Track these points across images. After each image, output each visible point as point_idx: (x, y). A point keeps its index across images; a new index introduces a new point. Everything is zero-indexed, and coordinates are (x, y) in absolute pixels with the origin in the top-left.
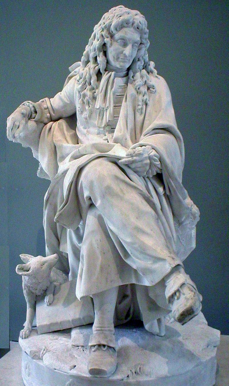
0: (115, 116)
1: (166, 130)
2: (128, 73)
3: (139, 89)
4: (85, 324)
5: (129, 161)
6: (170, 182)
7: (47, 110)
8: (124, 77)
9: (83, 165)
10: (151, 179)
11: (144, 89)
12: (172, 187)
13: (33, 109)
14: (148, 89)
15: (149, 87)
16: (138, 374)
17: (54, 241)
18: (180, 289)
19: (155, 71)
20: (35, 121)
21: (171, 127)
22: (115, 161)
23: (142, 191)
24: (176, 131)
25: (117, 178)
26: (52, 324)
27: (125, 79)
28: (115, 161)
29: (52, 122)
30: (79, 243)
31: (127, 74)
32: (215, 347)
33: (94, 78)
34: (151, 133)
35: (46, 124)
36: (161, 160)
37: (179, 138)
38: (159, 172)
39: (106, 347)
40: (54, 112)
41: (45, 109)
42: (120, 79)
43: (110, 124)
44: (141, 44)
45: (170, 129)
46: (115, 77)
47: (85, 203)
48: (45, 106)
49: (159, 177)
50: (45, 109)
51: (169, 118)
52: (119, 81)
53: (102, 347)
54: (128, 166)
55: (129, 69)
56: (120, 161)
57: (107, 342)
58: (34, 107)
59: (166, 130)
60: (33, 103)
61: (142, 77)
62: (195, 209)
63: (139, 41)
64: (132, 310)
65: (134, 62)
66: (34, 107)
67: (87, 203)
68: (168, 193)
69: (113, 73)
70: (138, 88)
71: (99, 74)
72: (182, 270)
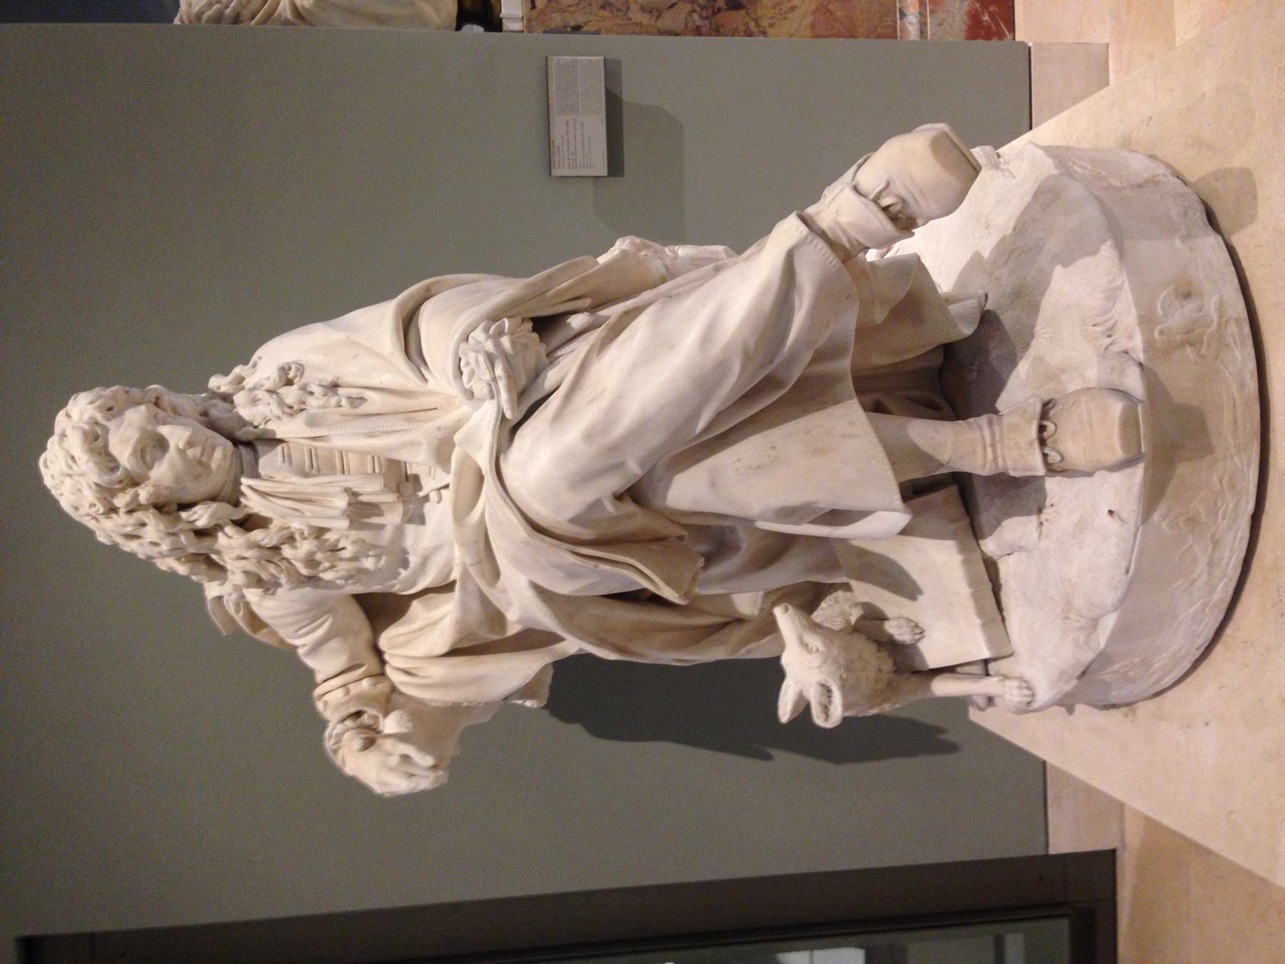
0: (370, 471)
1: (408, 324)
2: (250, 444)
3: (291, 407)
4: (967, 521)
5: (509, 389)
6: (558, 294)
7: (350, 686)
8: (255, 451)
9: (524, 522)
10: (552, 346)
11: (291, 395)
12: (569, 288)
13: (349, 723)
14: (289, 383)
15: (284, 380)
16: (1112, 328)
17: (737, 633)
18: (872, 197)
19: (238, 370)
20: (386, 714)
21: (401, 306)
22: (509, 430)
23: (592, 347)
24: (411, 296)
25: (558, 417)
26: (981, 613)
27: (260, 448)
28: (509, 430)
29: (388, 670)
30: (738, 549)
31: (249, 444)
32: (999, 156)
33: (257, 535)
34: (420, 363)
35: (394, 689)
36: (494, 317)
37: (428, 289)
38: (530, 325)
39: (1046, 423)
40: (359, 666)
41: (348, 692)
42: (262, 461)
43: (393, 485)
44: (157, 404)
45: (406, 312)
46: (256, 475)
47: (629, 516)
48: (340, 693)
49: (546, 325)
50: (348, 692)
51: (377, 322)
52: (269, 461)
53: (1046, 434)
54: (522, 394)
55: (236, 442)
56: (508, 415)
57: (1029, 421)
58: (343, 720)
59: (408, 324)
60: (331, 725)
61: (254, 401)
62: (621, 245)
63: (148, 409)
64: (915, 393)
65: (213, 426)
66: (343, 720)
67: (629, 507)
68: (587, 302)
69: (244, 480)
70: (288, 410)
71: (248, 523)
72: (811, 210)
